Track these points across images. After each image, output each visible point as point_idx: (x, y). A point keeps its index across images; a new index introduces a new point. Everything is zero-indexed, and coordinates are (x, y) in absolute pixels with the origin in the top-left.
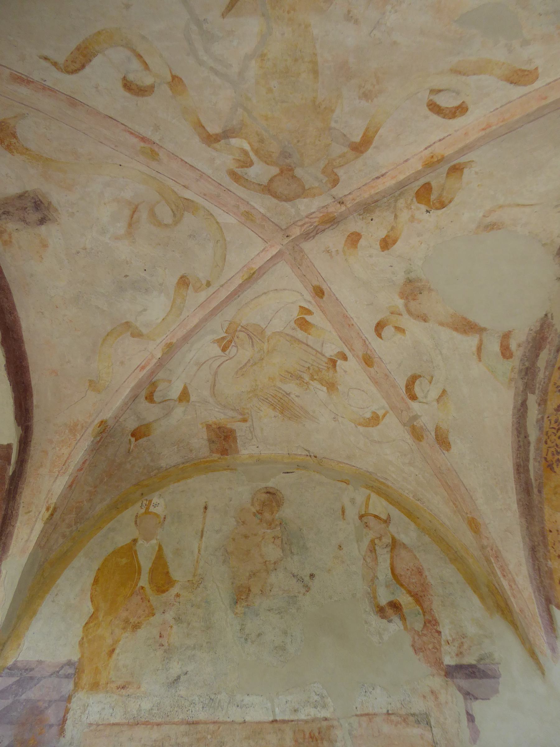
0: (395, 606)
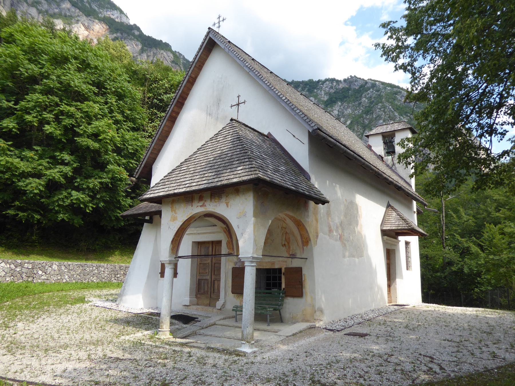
0: (285, 245)
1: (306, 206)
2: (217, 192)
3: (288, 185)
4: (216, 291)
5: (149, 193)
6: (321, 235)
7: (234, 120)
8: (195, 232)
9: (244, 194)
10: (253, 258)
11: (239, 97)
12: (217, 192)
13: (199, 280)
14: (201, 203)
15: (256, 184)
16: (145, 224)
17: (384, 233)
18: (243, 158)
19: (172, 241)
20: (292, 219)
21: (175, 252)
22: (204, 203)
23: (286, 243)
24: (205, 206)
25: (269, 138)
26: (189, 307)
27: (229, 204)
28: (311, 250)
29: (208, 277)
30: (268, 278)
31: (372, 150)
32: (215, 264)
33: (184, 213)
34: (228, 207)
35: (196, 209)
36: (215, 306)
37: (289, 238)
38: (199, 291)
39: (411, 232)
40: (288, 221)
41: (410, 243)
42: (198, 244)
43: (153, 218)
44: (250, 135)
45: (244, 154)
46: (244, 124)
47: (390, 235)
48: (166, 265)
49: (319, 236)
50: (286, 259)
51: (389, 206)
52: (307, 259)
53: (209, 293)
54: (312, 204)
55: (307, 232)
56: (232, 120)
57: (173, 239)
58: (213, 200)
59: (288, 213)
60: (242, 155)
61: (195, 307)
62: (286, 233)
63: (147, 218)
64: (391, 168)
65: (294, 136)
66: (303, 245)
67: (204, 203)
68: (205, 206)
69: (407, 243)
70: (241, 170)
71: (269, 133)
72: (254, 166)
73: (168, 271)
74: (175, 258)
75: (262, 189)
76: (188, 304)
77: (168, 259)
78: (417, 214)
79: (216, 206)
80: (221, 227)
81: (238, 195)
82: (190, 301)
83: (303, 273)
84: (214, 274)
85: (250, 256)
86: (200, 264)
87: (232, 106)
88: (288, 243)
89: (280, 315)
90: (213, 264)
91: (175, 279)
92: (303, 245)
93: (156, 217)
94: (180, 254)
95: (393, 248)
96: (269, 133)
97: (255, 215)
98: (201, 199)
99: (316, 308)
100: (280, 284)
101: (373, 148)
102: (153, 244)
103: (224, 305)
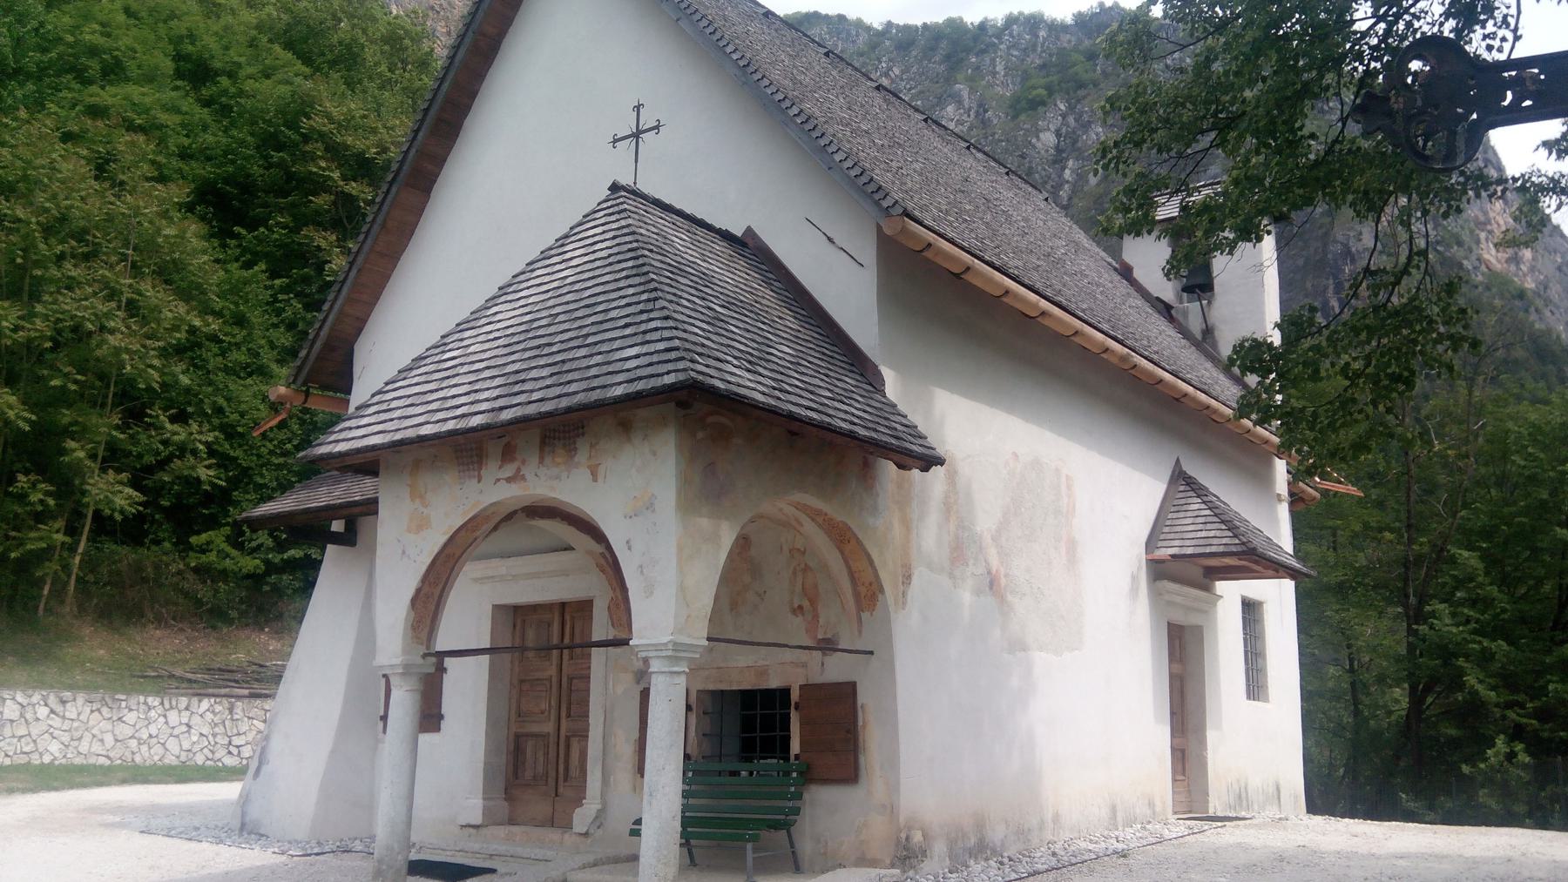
0: (800, 607)
1: (867, 473)
2: (562, 430)
3: (797, 404)
4: (574, 772)
5: (332, 438)
6: (920, 576)
7: (624, 188)
8: (503, 571)
9: (645, 437)
10: (677, 646)
11: (638, 108)
12: (562, 430)
13: (518, 736)
14: (509, 470)
15: (682, 405)
16: (329, 546)
17: (1161, 571)
18: (644, 317)
19: (414, 601)
20: (820, 520)
21: (424, 635)
22: (519, 470)
23: (806, 604)
24: (523, 478)
25: (748, 247)
26: (484, 831)
27: (601, 470)
28: (887, 622)
29: (548, 728)
30: (747, 724)
31: (1133, 282)
32: (570, 679)
33: (452, 503)
34: (595, 480)
35: (494, 489)
36: (568, 826)
37: (816, 586)
38: (516, 775)
39: (1252, 560)
40: (809, 527)
41: (1260, 604)
42: (515, 617)
43: (352, 527)
44: (680, 241)
45: (650, 306)
46: (657, 203)
47: (1184, 571)
48: (394, 681)
49: (915, 580)
50: (803, 656)
51: (1181, 481)
52: (871, 653)
53: (551, 782)
54: (888, 469)
55: (871, 562)
56: (615, 188)
57: (418, 591)
58: (548, 460)
59: (799, 497)
60: (641, 307)
61: (501, 831)
62: (807, 569)
63: (337, 526)
64: (1197, 345)
65: (830, 239)
66: (860, 609)
67: (519, 470)
68: (523, 478)
69: (1251, 609)
70: (637, 357)
71: (749, 230)
72: (677, 343)
73: (403, 702)
74: (425, 656)
75: (705, 418)
76: (478, 820)
77: (397, 661)
78: (1291, 504)
79: (558, 477)
80: (590, 553)
81: (629, 440)
82: (487, 812)
83: (861, 700)
84: (569, 716)
85: (665, 639)
86: (522, 681)
87: (615, 141)
88: (813, 602)
89: (792, 845)
90: (564, 680)
91: (425, 739)
92: (860, 609)
93: (364, 523)
94: (442, 644)
95: (1193, 619)
96: (749, 230)
97: (687, 505)
98: (508, 454)
99: (901, 819)
100: (786, 741)
101: (1137, 274)
102: (350, 621)
103: (600, 818)
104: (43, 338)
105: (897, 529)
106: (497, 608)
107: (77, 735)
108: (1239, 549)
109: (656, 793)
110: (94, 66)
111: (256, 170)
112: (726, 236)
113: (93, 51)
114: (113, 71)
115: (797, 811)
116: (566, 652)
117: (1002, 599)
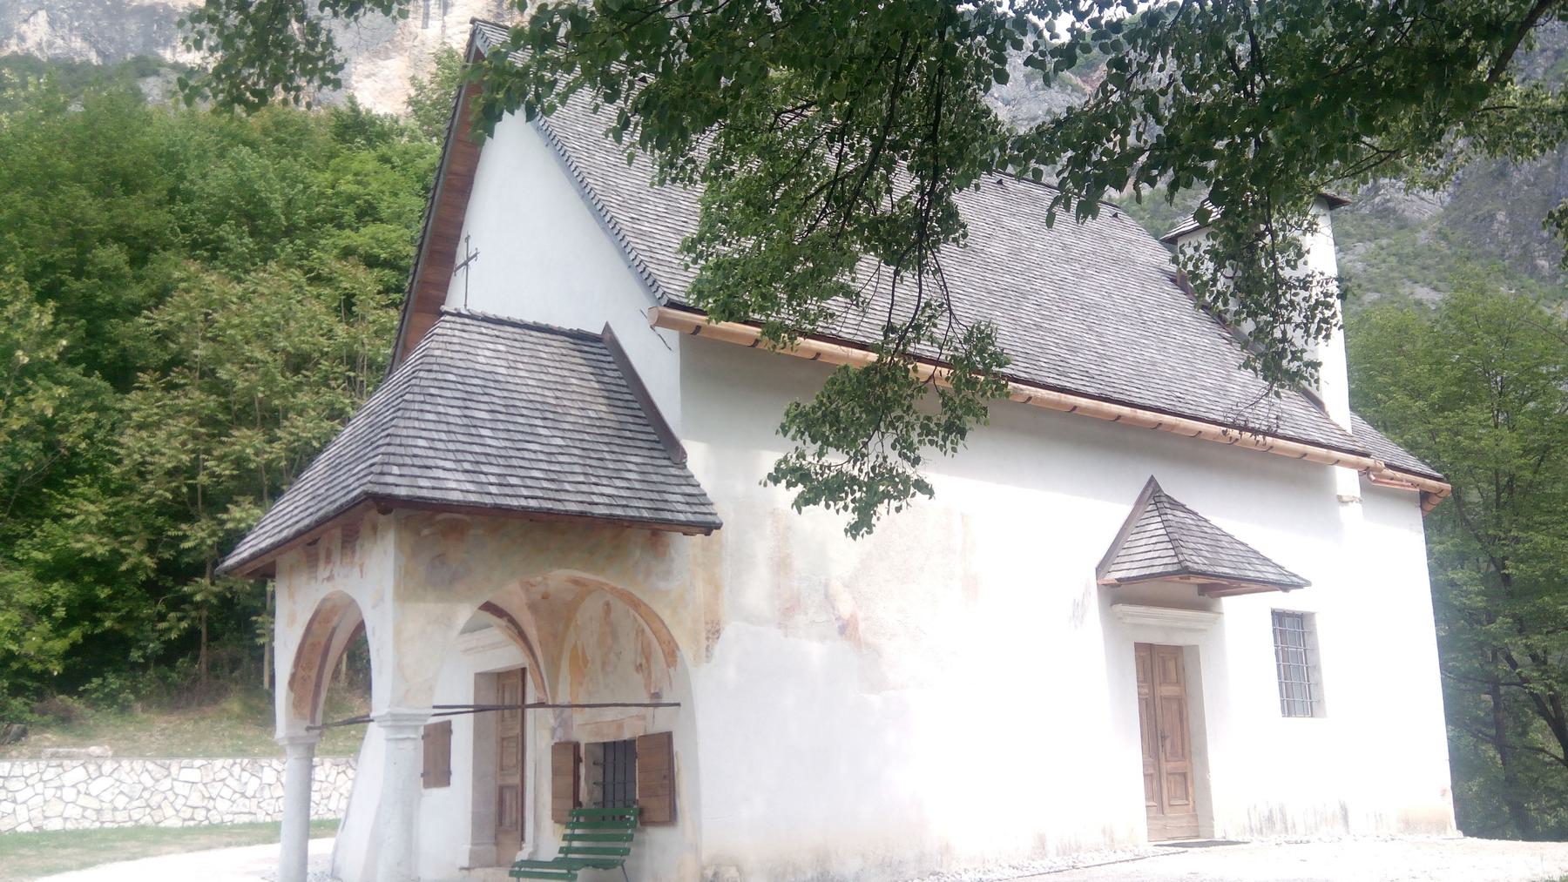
21: (307, 711)
74: (308, 729)
76: (466, 864)
104: (279, 459)
105: (700, 591)
106: (480, 676)
107: (326, 794)
108: (1176, 568)
109: (545, 838)
110: (350, 213)
111: (1486, 103)
112: (579, 337)
113: (351, 199)
114: (368, 213)
115: (627, 852)
116: (507, 712)
117: (858, 643)
